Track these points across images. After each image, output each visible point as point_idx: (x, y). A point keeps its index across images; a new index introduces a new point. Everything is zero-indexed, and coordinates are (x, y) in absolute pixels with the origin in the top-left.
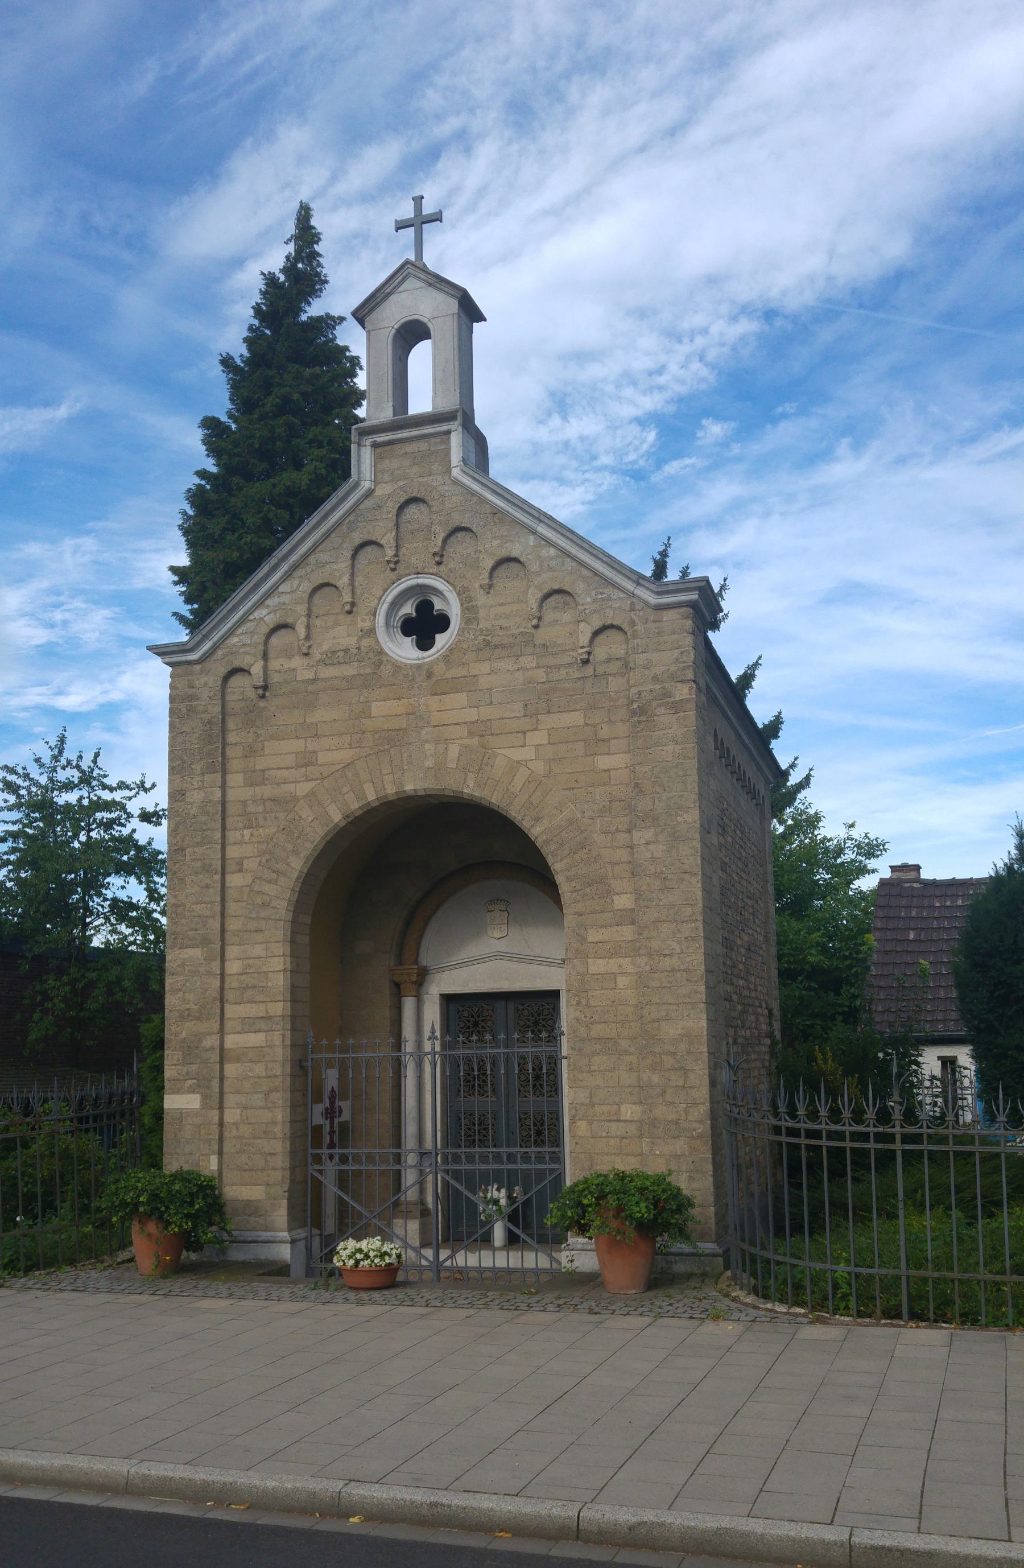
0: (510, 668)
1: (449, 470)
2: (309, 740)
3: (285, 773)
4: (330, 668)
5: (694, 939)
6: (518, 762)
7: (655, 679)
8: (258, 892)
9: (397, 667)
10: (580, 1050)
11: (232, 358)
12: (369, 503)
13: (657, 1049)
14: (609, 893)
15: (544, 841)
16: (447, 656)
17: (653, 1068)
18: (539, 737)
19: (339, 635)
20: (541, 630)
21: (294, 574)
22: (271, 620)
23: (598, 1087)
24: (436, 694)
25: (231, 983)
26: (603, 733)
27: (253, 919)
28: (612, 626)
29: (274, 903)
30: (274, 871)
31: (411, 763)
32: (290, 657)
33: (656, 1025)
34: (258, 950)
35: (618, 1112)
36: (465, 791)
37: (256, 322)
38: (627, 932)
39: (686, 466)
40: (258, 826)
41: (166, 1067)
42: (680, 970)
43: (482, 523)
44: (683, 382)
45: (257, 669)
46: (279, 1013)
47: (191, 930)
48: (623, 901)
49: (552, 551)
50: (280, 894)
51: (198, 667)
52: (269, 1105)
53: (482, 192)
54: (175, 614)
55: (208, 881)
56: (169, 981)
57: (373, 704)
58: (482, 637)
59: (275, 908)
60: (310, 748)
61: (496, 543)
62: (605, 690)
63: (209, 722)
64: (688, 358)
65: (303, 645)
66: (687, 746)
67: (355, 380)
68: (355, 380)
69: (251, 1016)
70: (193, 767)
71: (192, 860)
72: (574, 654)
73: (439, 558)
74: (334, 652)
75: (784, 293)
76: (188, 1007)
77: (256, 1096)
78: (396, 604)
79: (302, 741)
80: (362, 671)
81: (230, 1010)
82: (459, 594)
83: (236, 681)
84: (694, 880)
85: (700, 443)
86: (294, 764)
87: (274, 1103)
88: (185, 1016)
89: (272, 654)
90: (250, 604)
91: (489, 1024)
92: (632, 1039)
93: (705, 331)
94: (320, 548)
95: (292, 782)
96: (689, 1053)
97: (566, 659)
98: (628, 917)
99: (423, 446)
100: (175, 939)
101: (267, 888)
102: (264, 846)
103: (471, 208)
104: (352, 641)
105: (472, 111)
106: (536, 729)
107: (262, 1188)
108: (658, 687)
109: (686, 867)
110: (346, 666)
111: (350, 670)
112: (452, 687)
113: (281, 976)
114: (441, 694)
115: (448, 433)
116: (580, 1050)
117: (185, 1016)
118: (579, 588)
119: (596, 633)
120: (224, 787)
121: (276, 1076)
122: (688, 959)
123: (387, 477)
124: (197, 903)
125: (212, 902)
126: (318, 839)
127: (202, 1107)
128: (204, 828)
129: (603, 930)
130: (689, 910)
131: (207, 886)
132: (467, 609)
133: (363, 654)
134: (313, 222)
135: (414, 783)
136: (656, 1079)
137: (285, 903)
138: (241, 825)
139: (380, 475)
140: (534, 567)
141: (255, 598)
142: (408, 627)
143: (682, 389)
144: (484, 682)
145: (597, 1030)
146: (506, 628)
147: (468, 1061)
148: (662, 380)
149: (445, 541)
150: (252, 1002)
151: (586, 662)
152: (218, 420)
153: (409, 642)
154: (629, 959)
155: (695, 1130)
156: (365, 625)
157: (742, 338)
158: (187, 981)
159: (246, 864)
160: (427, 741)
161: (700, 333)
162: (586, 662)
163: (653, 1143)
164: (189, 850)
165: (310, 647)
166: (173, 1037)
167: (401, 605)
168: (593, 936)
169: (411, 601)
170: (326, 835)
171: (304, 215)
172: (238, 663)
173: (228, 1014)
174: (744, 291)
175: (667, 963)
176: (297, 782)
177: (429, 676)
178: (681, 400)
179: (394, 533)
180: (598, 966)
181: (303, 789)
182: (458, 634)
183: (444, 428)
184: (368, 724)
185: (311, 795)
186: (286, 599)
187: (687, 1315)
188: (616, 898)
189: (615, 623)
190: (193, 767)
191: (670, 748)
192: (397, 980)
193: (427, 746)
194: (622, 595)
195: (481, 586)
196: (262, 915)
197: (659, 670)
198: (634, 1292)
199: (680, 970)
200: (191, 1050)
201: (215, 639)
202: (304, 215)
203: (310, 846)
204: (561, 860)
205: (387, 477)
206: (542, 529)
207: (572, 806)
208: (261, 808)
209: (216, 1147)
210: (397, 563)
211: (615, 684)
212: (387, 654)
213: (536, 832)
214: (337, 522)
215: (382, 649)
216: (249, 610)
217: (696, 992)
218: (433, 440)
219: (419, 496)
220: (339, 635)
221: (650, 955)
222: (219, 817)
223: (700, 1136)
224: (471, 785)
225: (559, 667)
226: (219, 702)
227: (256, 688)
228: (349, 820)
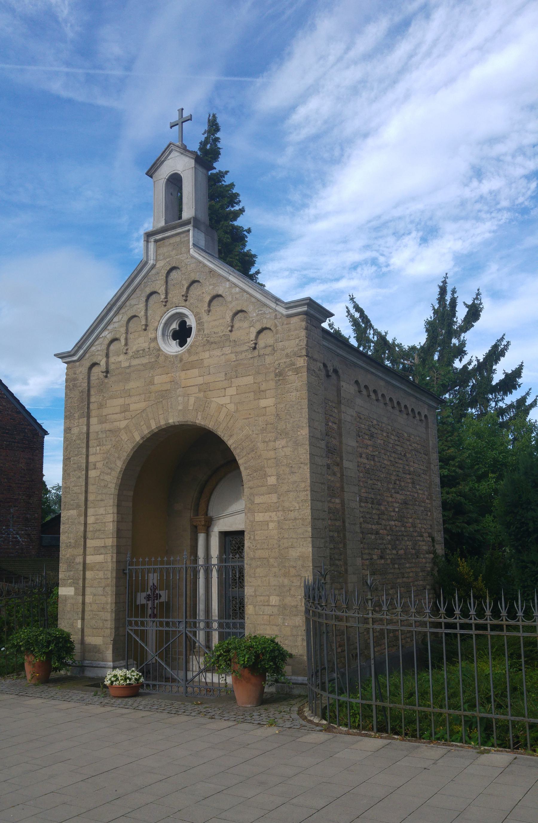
2: (126, 398)
4: (137, 360)
6: (222, 405)
7: (287, 356)
12: (153, 271)
13: (287, 565)
14: (265, 476)
18: (232, 391)
24: (184, 370)
26: (263, 388)
35: (268, 601)
36: (197, 422)
38: (274, 498)
40: (103, 445)
48: (272, 480)
51: (78, 363)
55: (79, 474)
56: (62, 527)
59: (109, 488)
61: (211, 287)
63: (82, 392)
66: (303, 392)
72: (249, 345)
73: (186, 297)
74: (138, 351)
80: (150, 361)
82: (195, 316)
84: (306, 467)
89: (111, 354)
97: (245, 348)
99: (177, 239)
100: (65, 505)
104: (146, 345)
106: (231, 387)
109: (302, 460)
113: (111, 524)
116: (250, 565)
117: (68, 546)
118: (250, 308)
122: (302, 513)
127: (75, 594)
128: (79, 446)
130: (303, 485)
131: (79, 477)
137: (114, 485)
138: (95, 445)
140: (229, 299)
141: (102, 326)
144: (206, 363)
146: (217, 333)
151: (255, 348)
154: (275, 513)
160: (179, 396)
164: (72, 458)
166: (63, 557)
170: (133, 448)
175: (292, 515)
176: (120, 421)
181: (123, 424)
184: (152, 387)
185: (127, 426)
186: (116, 325)
188: (268, 478)
191: (294, 394)
192: (195, 524)
194: (271, 311)
196: (104, 492)
197: (289, 351)
201: (85, 348)
203: (125, 454)
204: (242, 458)
207: (248, 428)
215: (160, 348)
217: (307, 531)
218: (182, 235)
222: (85, 441)
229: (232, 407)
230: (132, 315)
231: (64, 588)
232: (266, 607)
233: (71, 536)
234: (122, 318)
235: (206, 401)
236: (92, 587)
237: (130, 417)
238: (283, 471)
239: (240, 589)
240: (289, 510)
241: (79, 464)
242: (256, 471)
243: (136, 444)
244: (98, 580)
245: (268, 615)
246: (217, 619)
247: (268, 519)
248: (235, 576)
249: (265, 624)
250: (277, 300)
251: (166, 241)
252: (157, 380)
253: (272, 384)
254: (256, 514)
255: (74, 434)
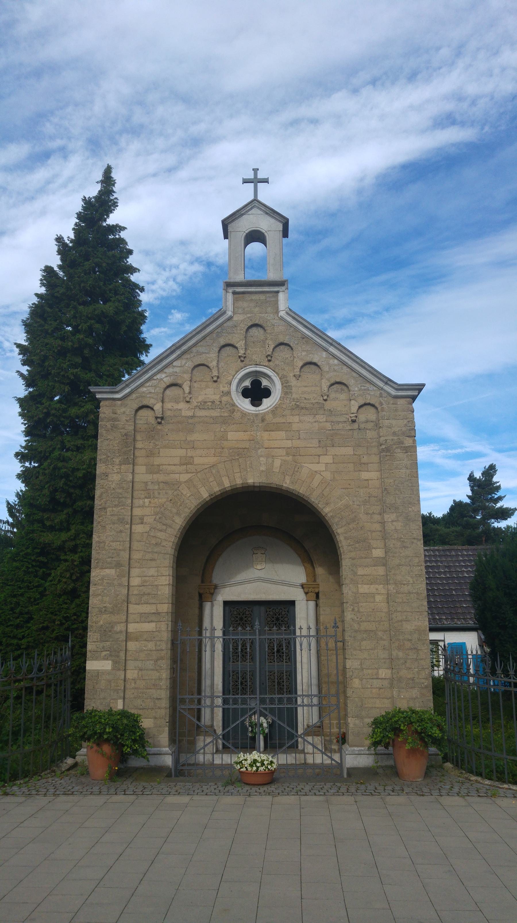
0: (310, 420)
1: (277, 312)
2: (189, 450)
3: (173, 468)
4: (203, 411)
5: (420, 576)
6: (316, 472)
7: (394, 434)
8: (153, 537)
9: (244, 414)
10: (354, 637)
11: (63, 238)
12: (229, 323)
13: (401, 638)
14: (369, 548)
15: (331, 516)
16: (274, 410)
17: (399, 648)
18: (328, 459)
19: (209, 393)
20: (327, 402)
21: (183, 356)
22: (168, 380)
23: (365, 659)
24: (267, 431)
25: (134, 591)
27: (149, 552)
28: (369, 404)
29: (164, 543)
30: (164, 525)
31: (252, 467)
32: (178, 403)
33: (400, 623)
34: (152, 572)
35: (377, 674)
36: (284, 485)
37: (78, 221)
38: (381, 571)
39: (161, 332)
40: (154, 497)
41: (88, 643)
42: (413, 593)
43: (296, 342)
44: (164, 290)
45: (158, 407)
46: (165, 611)
47: (109, 558)
48: (378, 553)
49: (336, 361)
50: (169, 539)
51: (119, 402)
52: (158, 668)
53: (71, 179)
54: (424, 385)
55: (122, 528)
56: (92, 589)
57: (229, 433)
58: (294, 403)
59: (163, 546)
60: (189, 454)
61: (304, 353)
62: (365, 437)
63: (126, 435)
64: (168, 279)
65: (187, 396)
66: (413, 470)
67: (128, 260)
68: (128, 260)
69: (146, 612)
70: (114, 460)
71: (111, 515)
72: (347, 416)
73: (269, 358)
74: (205, 402)
75: (217, 255)
76: (105, 605)
77: (148, 662)
78: (242, 380)
79: (184, 450)
80: (222, 414)
81: (132, 608)
82: (280, 379)
83: (143, 413)
84: (419, 543)
85: (169, 321)
86: (179, 463)
87: (161, 667)
88: (103, 611)
89: (166, 400)
90: (155, 370)
91: (269, 619)
92: (385, 631)
93: (177, 267)
94: (199, 344)
95: (178, 473)
96: (419, 640)
97: (342, 419)
98: (383, 562)
99: (262, 297)
100: (97, 563)
101: (159, 534)
102: (158, 510)
103: (64, 185)
104: (217, 397)
105: (69, 138)
106: (326, 455)
107: (152, 720)
108: (395, 438)
109: (415, 535)
110: (213, 411)
111: (215, 413)
112: (277, 427)
113: (167, 587)
114: (270, 431)
115: (278, 292)
116: (354, 637)
117: (103, 611)
118: (351, 382)
119: (360, 407)
120: (133, 473)
121: (163, 650)
122: (417, 587)
123: (240, 311)
124: (113, 541)
125: (124, 541)
126: (193, 507)
127: (113, 669)
128: (120, 496)
129: (367, 568)
130: (416, 560)
131: (121, 531)
132: (286, 386)
133: (223, 405)
134: (113, 175)
135: (253, 479)
136: (401, 654)
137: (171, 544)
138: (143, 496)
139: (236, 310)
140: (326, 368)
141: (159, 367)
142: (246, 393)
143: (164, 294)
144: (295, 427)
145: (365, 626)
146: (308, 399)
147: (271, 641)
148: (154, 287)
149: (273, 350)
150: (147, 603)
151: (354, 421)
152: (53, 268)
153: (248, 401)
154: (382, 585)
155: (423, 683)
156: (225, 389)
157: (195, 273)
158: (105, 589)
159: (146, 519)
160: (262, 456)
161: (175, 267)
162: (354, 421)
163: (399, 691)
164: (109, 509)
165: (191, 398)
166: (94, 625)
167: (244, 381)
168: (361, 571)
169: (249, 379)
170: (198, 505)
171: (108, 171)
172: (145, 402)
173: (131, 611)
174: (198, 251)
175: (406, 589)
176: (180, 473)
177: (263, 420)
178: (163, 298)
179: (244, 342)
180: (364, 589)
181: (184, 477)
182: (280, 399)
183: (276, 289)
184: (225, 444)
185: (190, 480)
187: (204, 793)
188: (373, 550)
189: (371, 402)
190: (114, 460)
191: (403, 471)
192: (201, 592)
193: (261, 459)
194: (375, 388)
195: (294, 376)
196: (155, 550)
197: (396, 429)
198: (420, 780)
199: (413, 593)
200: (106, 632)
201: (133, 387)
202: (108, 171)
203: (187, 511)
204: (341, 527)
205: (240, 311)
206: (332, 349)
207: (347, 498)
208: (156, 487)
209: (122, 695)
210: (245, 357)
211: (370, 434)
212: (237, 406)
213: (326, 511)
214: (211, 331)
215: (234, 403)
216: (155, 373)
217: (422, 605)
218: (268, 295)
219: (259, 323)
220: (209, 393)
221: (396, 584)
222: (130, 490)
223: (426, 687)
224: (288, 482)
225: (338, 422)
226: (133, 424)
227: (157, 418)
228: (212, 497)
229: (328, 475)
230: (199, 363)
231: (95, 663)
232: (374, 681)
233: (107, 599)
234: (186, 363)
235: (296, 465)
236: (136, 660)
237: (195, 471)
238: (394, 544)
239: (244, 663)
240: (401, 584)
241: (121, 517)
242: (358, 542)
243: (203, 501)
244: (146, 652)
245: (377, 688)
246: (221, 695)
247: (374, 591)
248: (237, 649)
249: (373, 698)
250: (388, 381)
251: (247, 296)
252: (231, 435)
253: (375, 459)
254: (359, 586)
255: (112, 481)
